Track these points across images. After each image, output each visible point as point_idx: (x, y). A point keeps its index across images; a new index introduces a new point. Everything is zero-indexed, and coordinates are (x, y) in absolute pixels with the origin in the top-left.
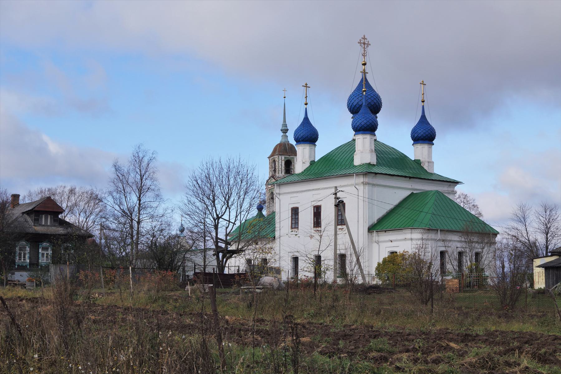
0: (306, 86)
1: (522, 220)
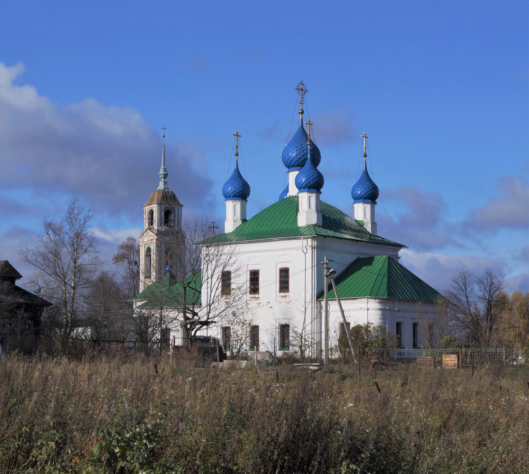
0: (237, 135)
1: (463, 287)
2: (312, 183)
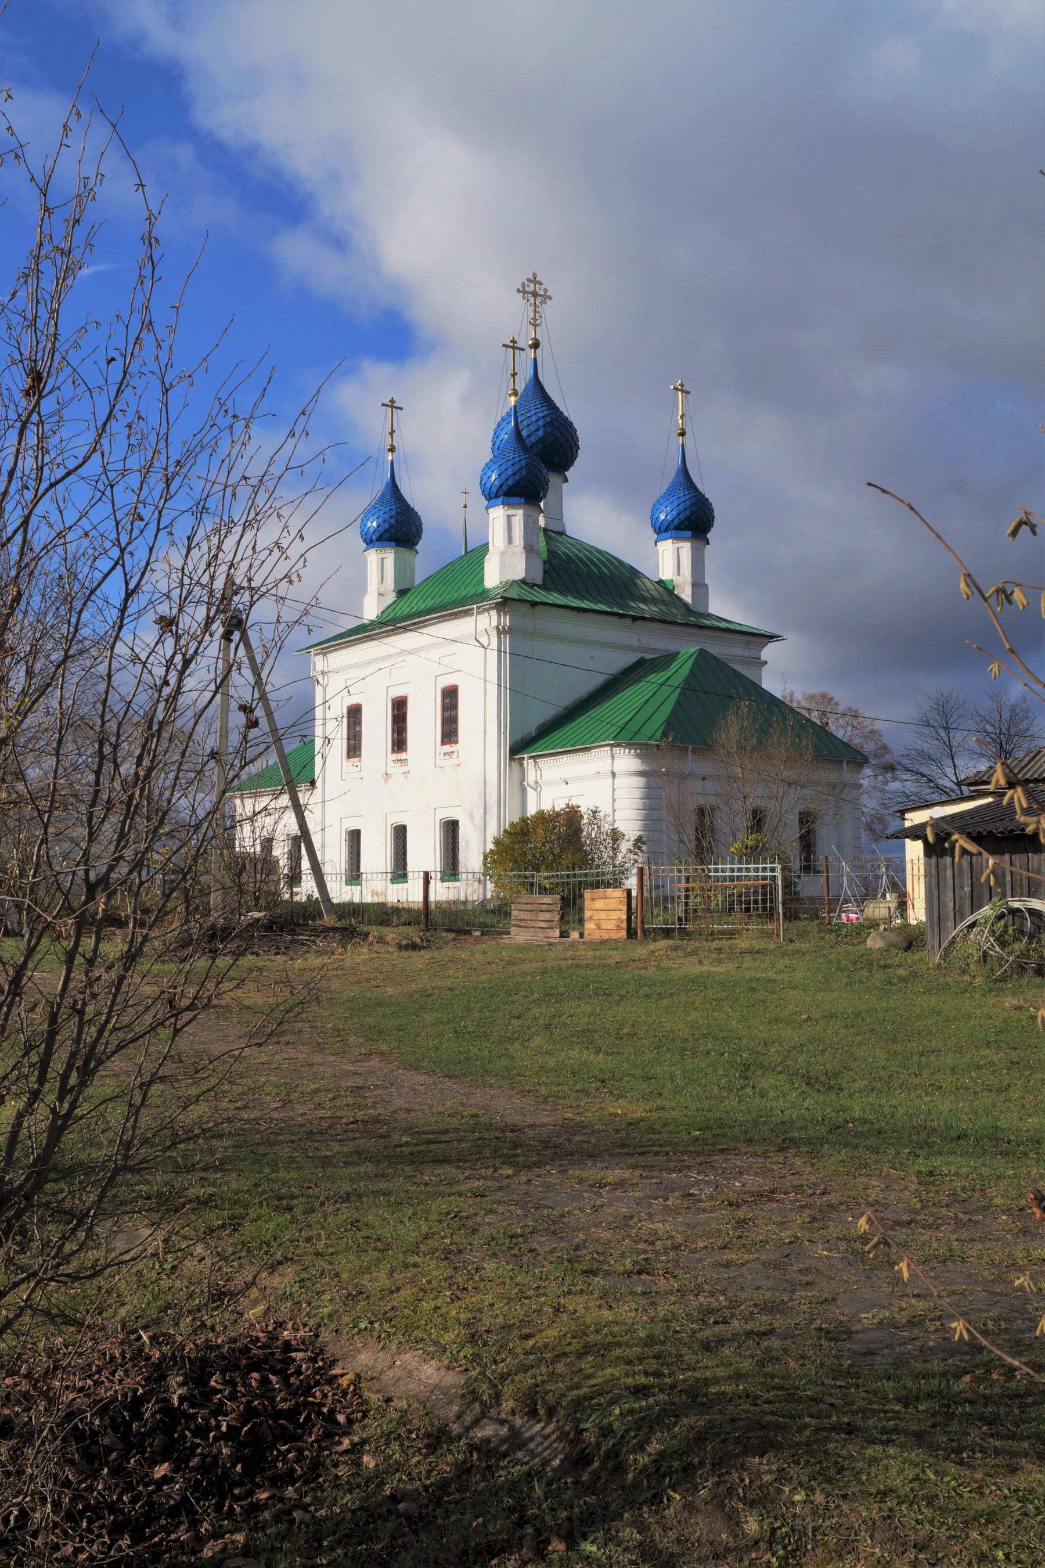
2: (511, 482)
